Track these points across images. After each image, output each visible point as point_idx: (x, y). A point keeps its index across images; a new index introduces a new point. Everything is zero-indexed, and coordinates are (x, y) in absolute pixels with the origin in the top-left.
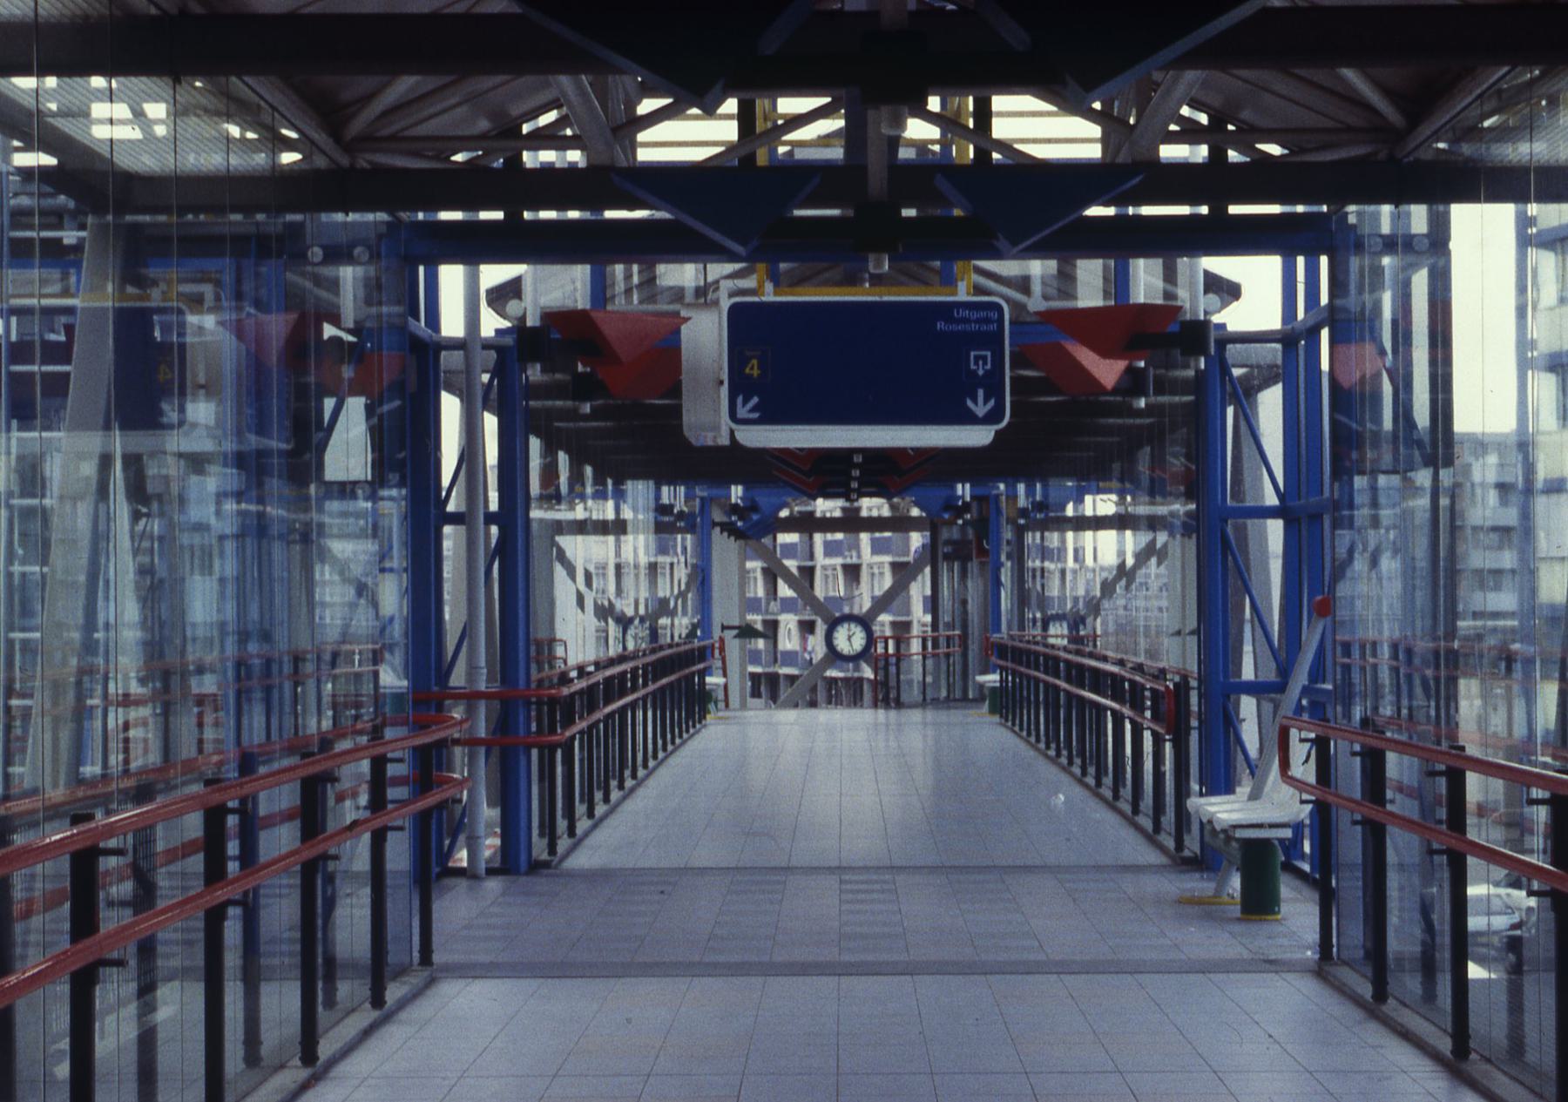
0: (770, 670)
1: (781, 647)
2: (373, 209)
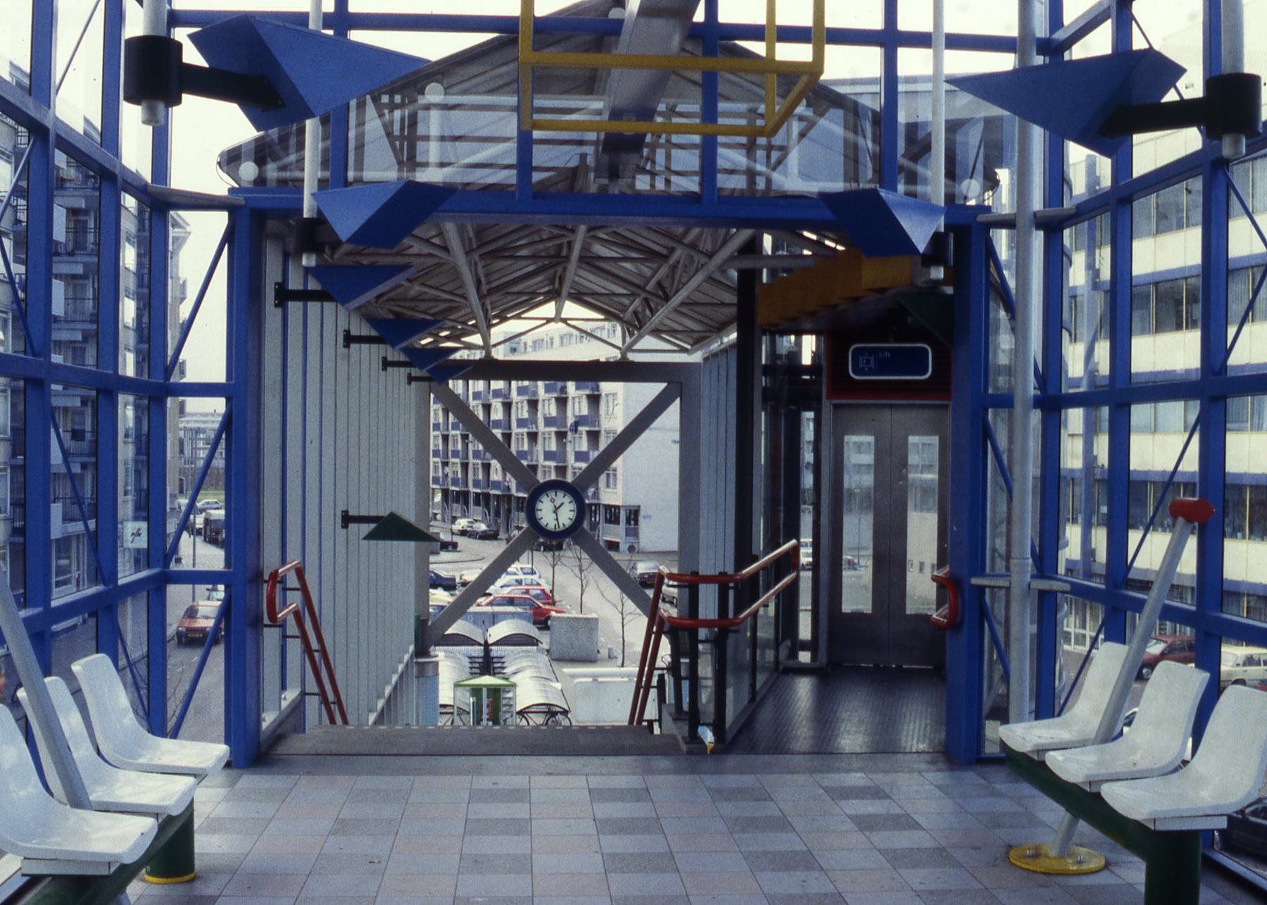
0: (485, 491)
1: (491, 479)
2: (1227, 619)
